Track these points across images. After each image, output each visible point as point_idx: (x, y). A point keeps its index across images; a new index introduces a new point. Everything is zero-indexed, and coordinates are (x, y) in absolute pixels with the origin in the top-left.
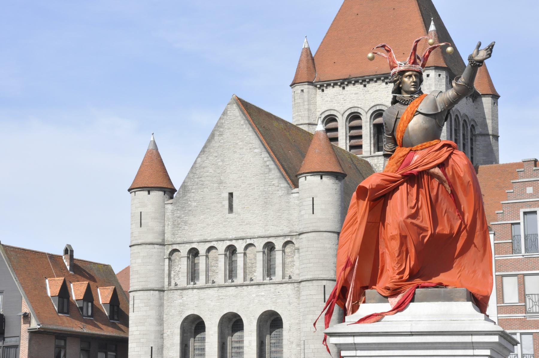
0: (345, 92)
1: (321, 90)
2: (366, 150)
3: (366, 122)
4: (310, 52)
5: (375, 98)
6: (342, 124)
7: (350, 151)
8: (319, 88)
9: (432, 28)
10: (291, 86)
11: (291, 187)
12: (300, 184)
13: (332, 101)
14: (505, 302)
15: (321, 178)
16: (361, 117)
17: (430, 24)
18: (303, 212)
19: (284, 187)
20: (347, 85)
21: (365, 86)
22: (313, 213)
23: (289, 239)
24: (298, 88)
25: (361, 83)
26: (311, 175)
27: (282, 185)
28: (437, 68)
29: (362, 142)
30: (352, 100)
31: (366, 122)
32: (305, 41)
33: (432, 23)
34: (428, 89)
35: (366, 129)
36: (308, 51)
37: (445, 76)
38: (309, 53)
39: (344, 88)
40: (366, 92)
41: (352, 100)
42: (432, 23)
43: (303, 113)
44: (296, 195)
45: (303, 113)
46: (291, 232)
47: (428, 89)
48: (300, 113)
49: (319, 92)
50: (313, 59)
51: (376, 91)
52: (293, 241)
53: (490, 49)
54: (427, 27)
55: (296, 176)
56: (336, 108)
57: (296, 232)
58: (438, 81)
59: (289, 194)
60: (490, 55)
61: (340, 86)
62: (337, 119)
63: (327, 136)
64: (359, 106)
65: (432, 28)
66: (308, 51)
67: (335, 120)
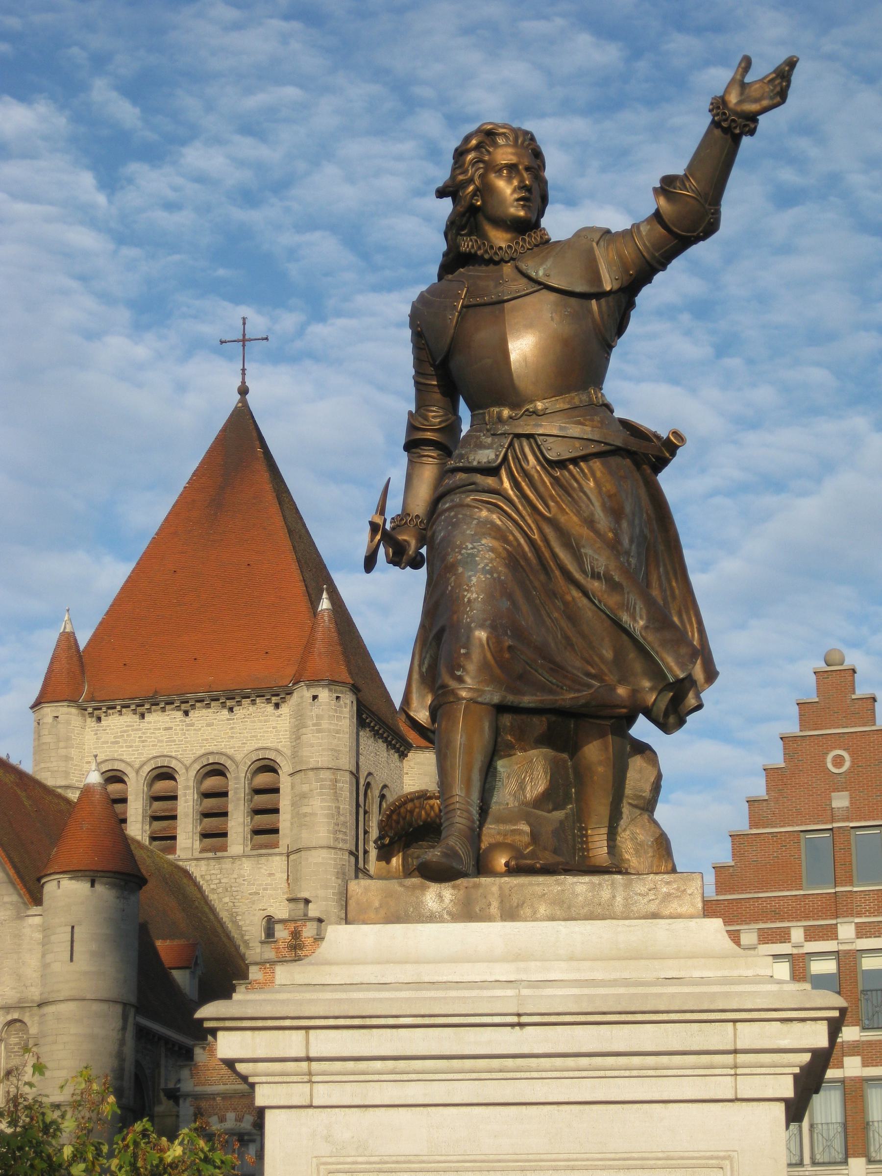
0: (144, 725)
1: (94, 719)
2: (183, 846)
3: (187, 788)
4: (76, 640)
5: (207, 740)
6: (238, 786)
7: (150, 843)
8: (91, 715)
9: (325, 604)
10: (32, 707)
11: (25, 903)
12: (46, 898)
13: (117, 743)
14: (853, 926)
15: (93, 885)
16: (177, 776)
17: (320, 598)
18: (49, 958)
19: (11, 903)
20: (149, 711)
21: (186, 713)
22: (72, 960)
23: (16, 1016)
24: (48, 711)
25: (178, 708)
26: (71, 879)
27: (7, 899)
28: (332, 683)
29: (175, 828)
30: (159, 741)
31: (187, 788)
32: (66, 618)
33: (325, 595)
34: (314, 725)
35: (186, 802)
36: (68, 640)
37: (348, 702)
38: (72, 643)
39: (143, 716)
40: (188, 725)
41: (159, 741)
42: (325, 595)
43: (55, 764)
44: (37, 920)
45: (55, 764)
46: (20, 1001)
47: (314, 725)
48: (48, 765)
49: (91, 722)
50: (80, 656)
51: (208, 725)
52: (26, 1020)
53: (783, 76)
54: (314, 602)
55: (39, 880)
56: (124, 757)
57: (33, 1001)
58: (336, 711)
59: (20, 917)
60: (782, 96)
61: (134, 712)
62: (126, 779)
63: (108, 794)
64: (173, 754)
65: (325, 604)
66: (68, 640)
67: (120, 780)
